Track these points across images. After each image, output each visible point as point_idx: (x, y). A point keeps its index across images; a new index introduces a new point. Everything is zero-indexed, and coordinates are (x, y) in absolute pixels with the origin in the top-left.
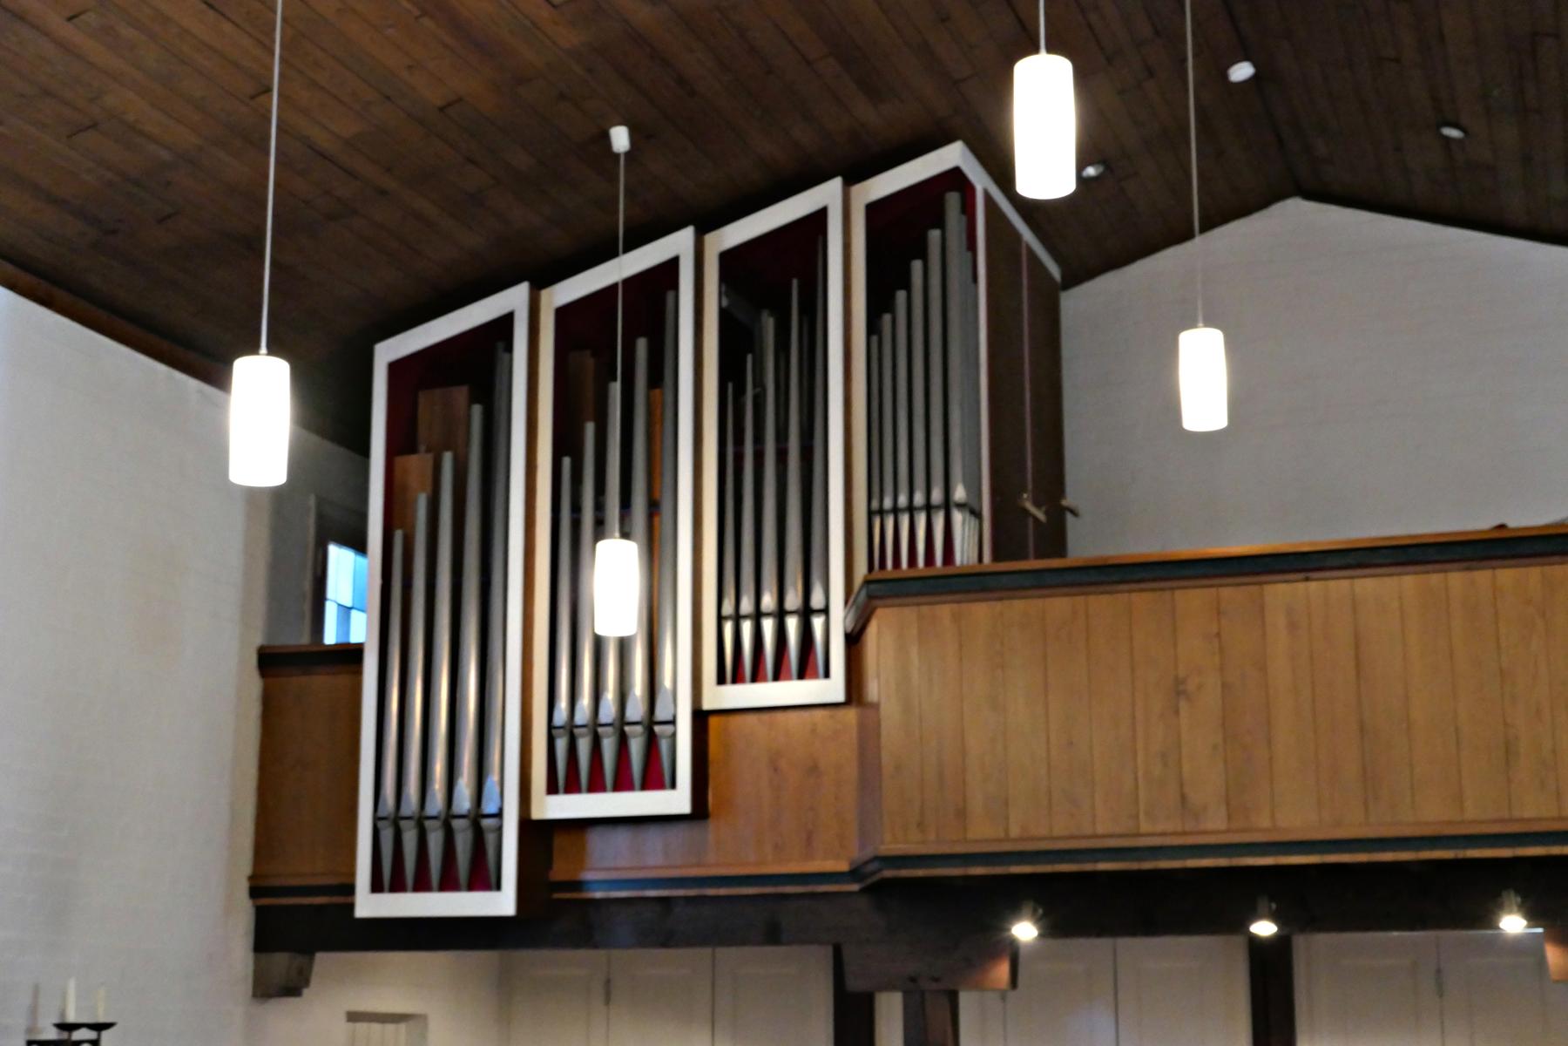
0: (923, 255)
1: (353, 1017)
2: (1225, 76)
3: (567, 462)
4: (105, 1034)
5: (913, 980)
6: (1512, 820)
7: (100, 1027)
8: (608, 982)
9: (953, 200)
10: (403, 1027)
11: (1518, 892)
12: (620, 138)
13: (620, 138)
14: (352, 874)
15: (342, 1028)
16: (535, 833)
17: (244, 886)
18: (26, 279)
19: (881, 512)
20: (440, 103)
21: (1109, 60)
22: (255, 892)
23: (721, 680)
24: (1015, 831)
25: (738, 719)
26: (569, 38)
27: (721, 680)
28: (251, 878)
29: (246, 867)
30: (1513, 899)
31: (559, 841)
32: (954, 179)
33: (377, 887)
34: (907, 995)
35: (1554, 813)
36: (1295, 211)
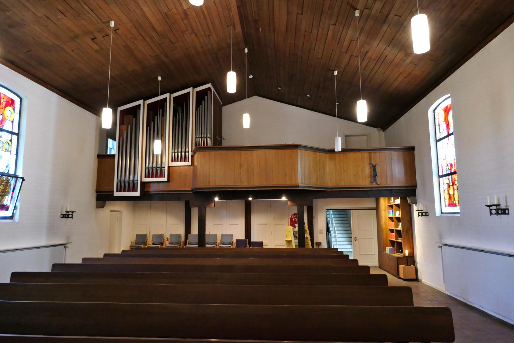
1: (111, 211)
12: (160, 78)
16: (143, 184)
29: (95, 188)
33: (117, 191)
36: (256, 97)
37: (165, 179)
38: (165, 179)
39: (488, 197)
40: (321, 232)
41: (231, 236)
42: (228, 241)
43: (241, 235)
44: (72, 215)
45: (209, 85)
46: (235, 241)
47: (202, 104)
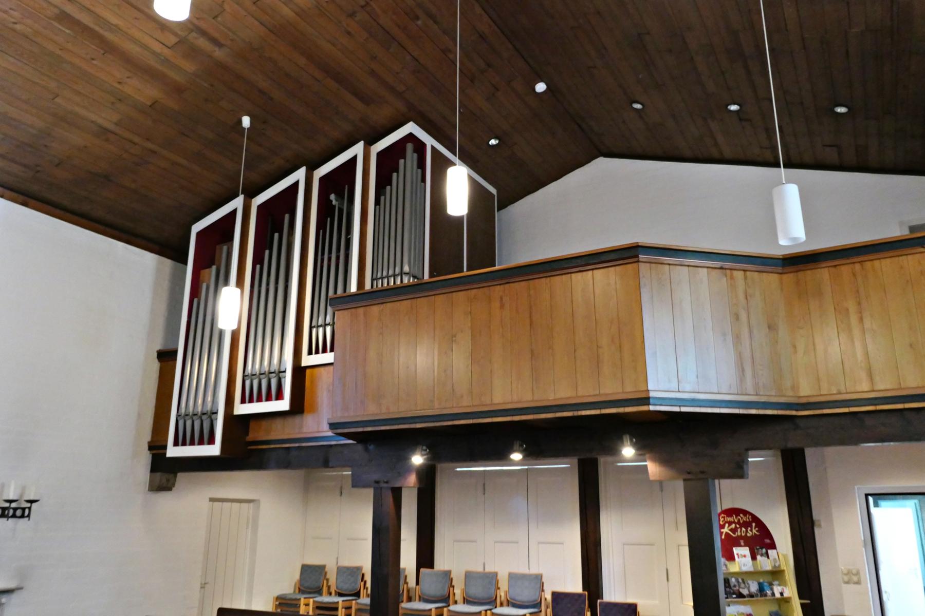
0: (397, 171)
1: (212, 500)
2: (534, 89)
3: (258, 267)
4: (34, 505)
5: (377, 482)
6: (600, 395)
7: (32, 502)
8: (341, 488)
9: (410, 147)
10: (251, 505)
11: (632, 436)
12: (246, 121)
13: (246, 121)
14: (167, 441)
15: (205, 505)
16: (231, 420)
17: (146, 447)
18: (21, 198)
19: (377, 279)
20: (149, 103)
21: (472, 81)
22: (151, 448)
23: (310, 353)
24: (384, 410)
25: (316, 370)
26: (189, 67)
27: (310, 353)
28: (149, 443)
29: (148, 437)
30: (627, 438)
31: (252, 424)
32: (411, 137)
33: (176, 444)
34: (375, 489)
35: (620, 390)
36: (601, 163)
37: (284, 405)
38: (284, 405)
39: (808, 601)
40: (852, 578)
41: (538, 580)
42: (526, 595)
43: (572, 583)
44: (30, 508)
45: (410, 128)
46: (549, 597)
47: (391, 184)
